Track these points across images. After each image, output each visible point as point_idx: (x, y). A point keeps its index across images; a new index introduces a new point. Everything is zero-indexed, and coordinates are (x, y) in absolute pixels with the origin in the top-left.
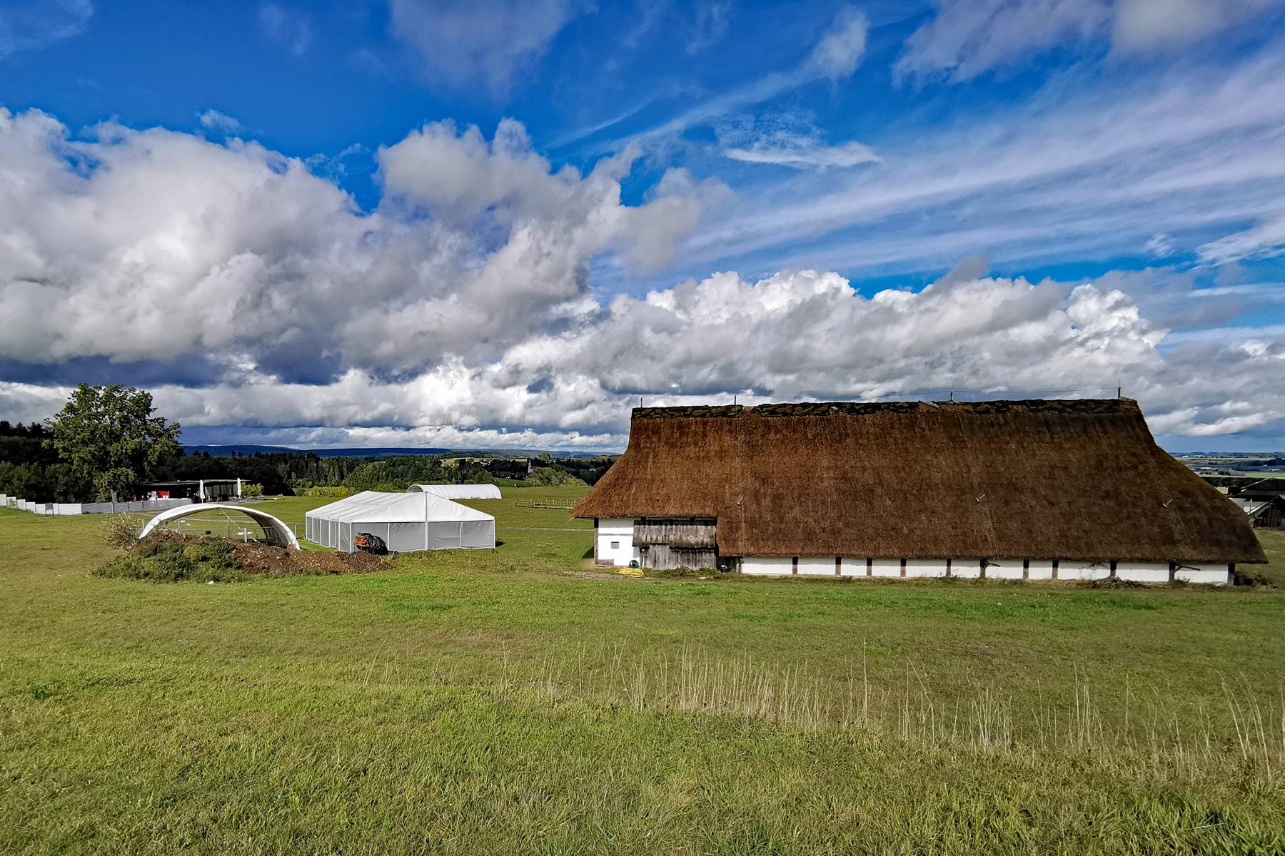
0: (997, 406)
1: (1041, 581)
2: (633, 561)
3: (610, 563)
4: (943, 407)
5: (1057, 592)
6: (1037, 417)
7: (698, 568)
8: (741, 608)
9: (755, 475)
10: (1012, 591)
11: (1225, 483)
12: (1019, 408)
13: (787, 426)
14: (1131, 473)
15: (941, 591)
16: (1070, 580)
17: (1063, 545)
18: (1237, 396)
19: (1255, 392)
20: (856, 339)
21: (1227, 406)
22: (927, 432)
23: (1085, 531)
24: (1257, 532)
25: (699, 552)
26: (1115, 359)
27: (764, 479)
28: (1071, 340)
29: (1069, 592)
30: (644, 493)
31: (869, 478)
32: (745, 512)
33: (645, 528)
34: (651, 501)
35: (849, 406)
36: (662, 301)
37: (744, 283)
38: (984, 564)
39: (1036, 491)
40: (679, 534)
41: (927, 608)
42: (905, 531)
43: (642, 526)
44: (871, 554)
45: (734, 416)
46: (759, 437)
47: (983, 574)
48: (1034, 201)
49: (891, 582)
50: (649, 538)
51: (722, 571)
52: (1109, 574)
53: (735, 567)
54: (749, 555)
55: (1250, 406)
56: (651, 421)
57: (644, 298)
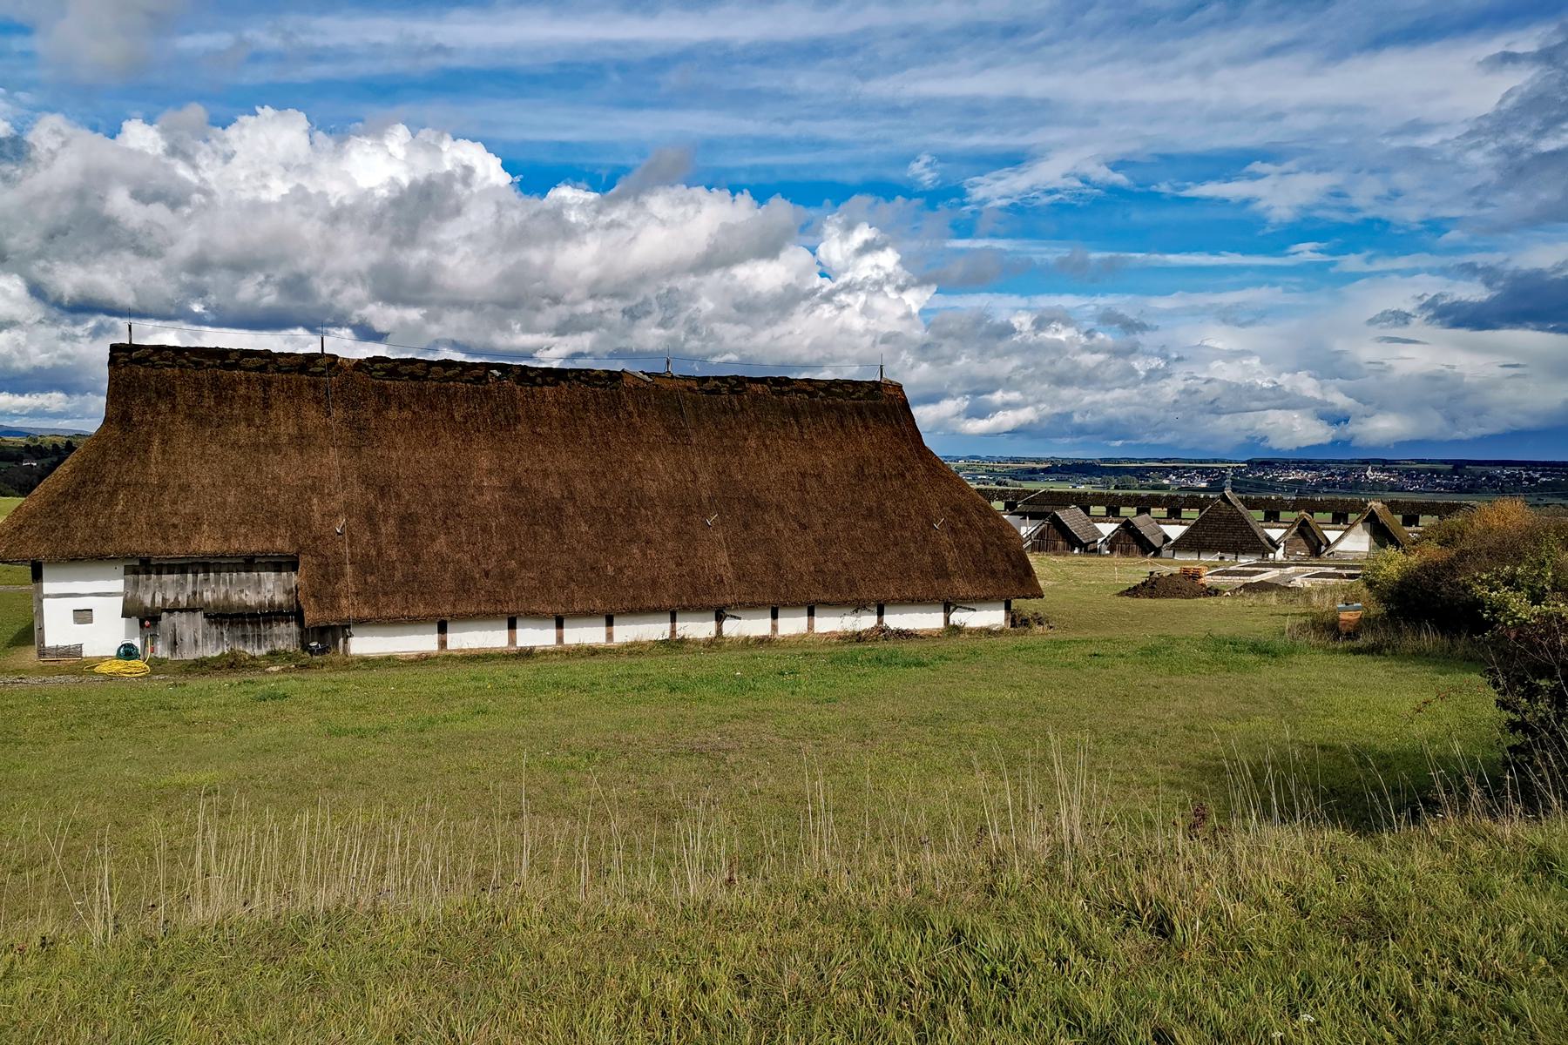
0: (730, 384)
1: (794, 636)
2: (124, 645)
3: (74, 652)
4: (658, 381)
5: (811, 651)
6: (782, 402)
7: (264, 651)
8: (345, 718)
9: (366, 480)
10: (756, 653)
11: (1001, 496)
12: (759, 388)
13: (419, 396)
14: (897, 483)
15: (661, 660)
16: (830, 633)
17: (819, 584)
18: (1007, 383)
19: (1026, 378)
20: (512, 259)
21: (998, 397)
22: (636, 419)
23: (845, 564)
24: (1032, 559)
25: (264, 623)
26: (873, 324)
27: (382, 489)
28: (814, 292)
29: (827, 650)
30: (144, 513)
31: (553, 489)
32: (350, 546)
33: (148, 579)
34: (160, 527)
35: (518, 372)
36: (141, 137)
37: (320, 135)
38: (720, 618)
39: (782, 509)
40: (223, 589)
41: (641, 688)
42: (610, 571)
43: (142, 577)
44: (560, 610)
45: (321, 374)
46: (369, 414)
47: (719, 631)
48: (765, 79)
49: (593, 652)
50: (159, 599)
51: (312, 652)
52: (876, 622)
53: (337, 644)
54: (362, 622)
55: (1021, 397)
56: (155, 372)
57: (114, 132)
